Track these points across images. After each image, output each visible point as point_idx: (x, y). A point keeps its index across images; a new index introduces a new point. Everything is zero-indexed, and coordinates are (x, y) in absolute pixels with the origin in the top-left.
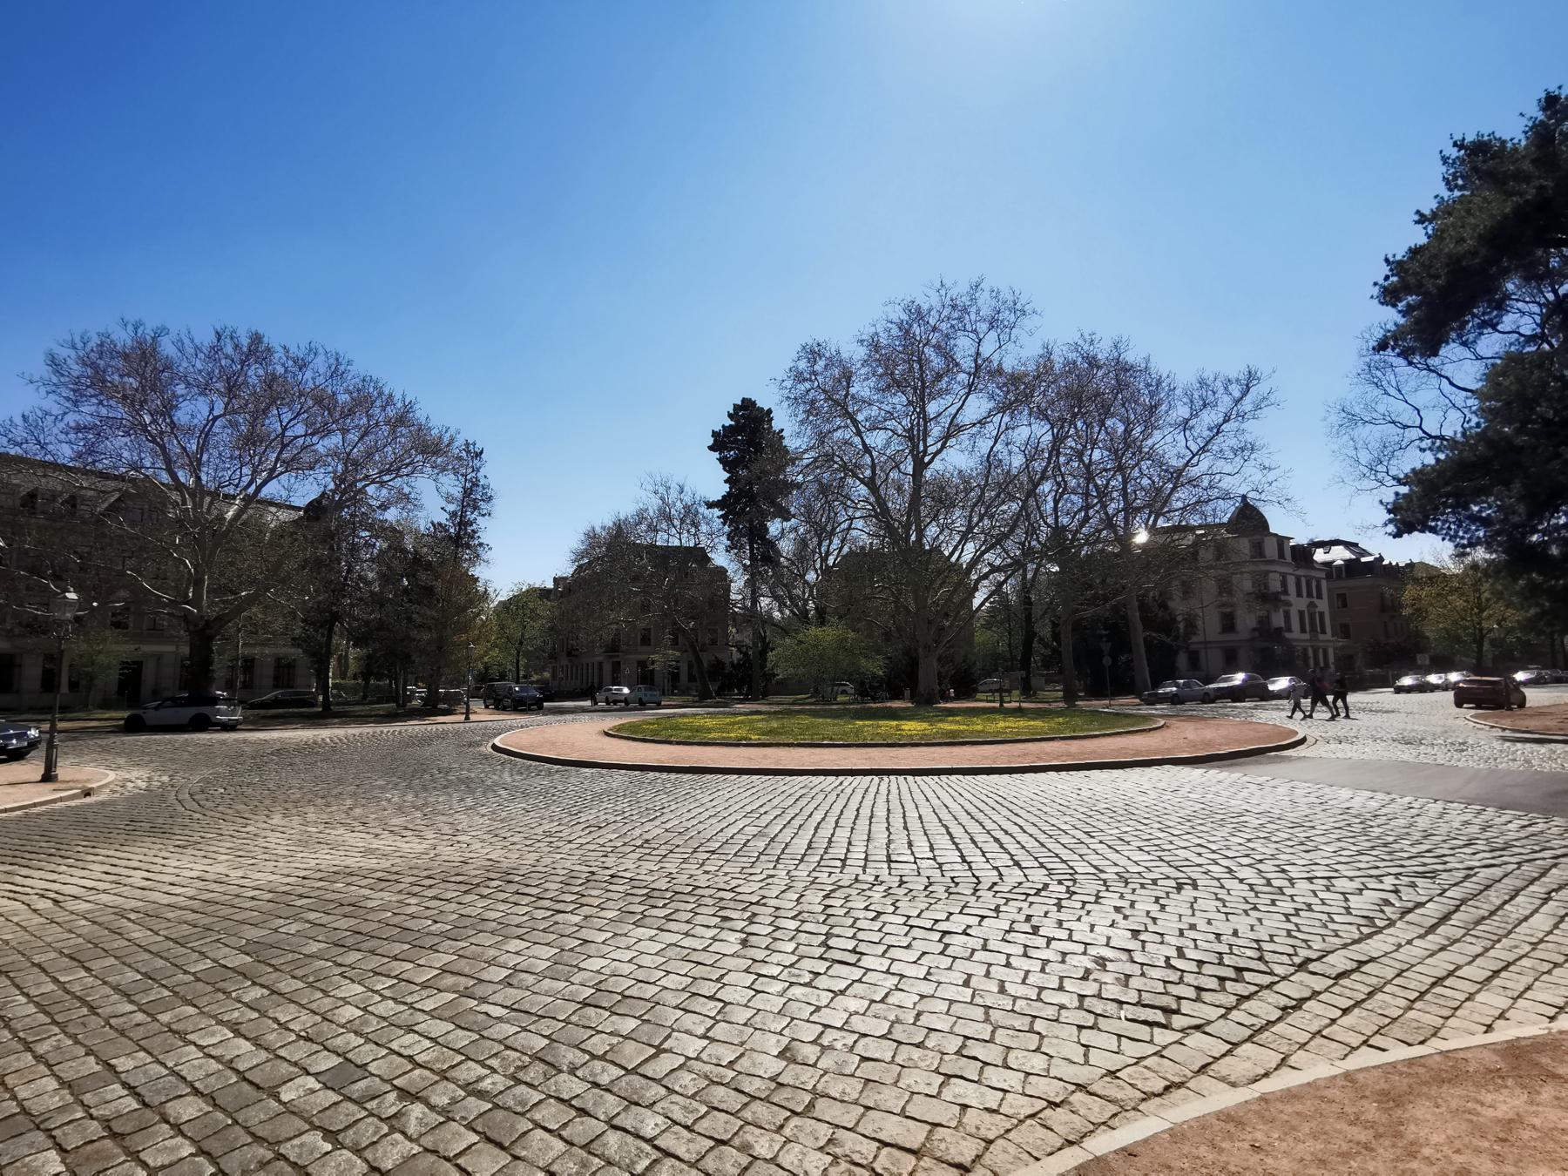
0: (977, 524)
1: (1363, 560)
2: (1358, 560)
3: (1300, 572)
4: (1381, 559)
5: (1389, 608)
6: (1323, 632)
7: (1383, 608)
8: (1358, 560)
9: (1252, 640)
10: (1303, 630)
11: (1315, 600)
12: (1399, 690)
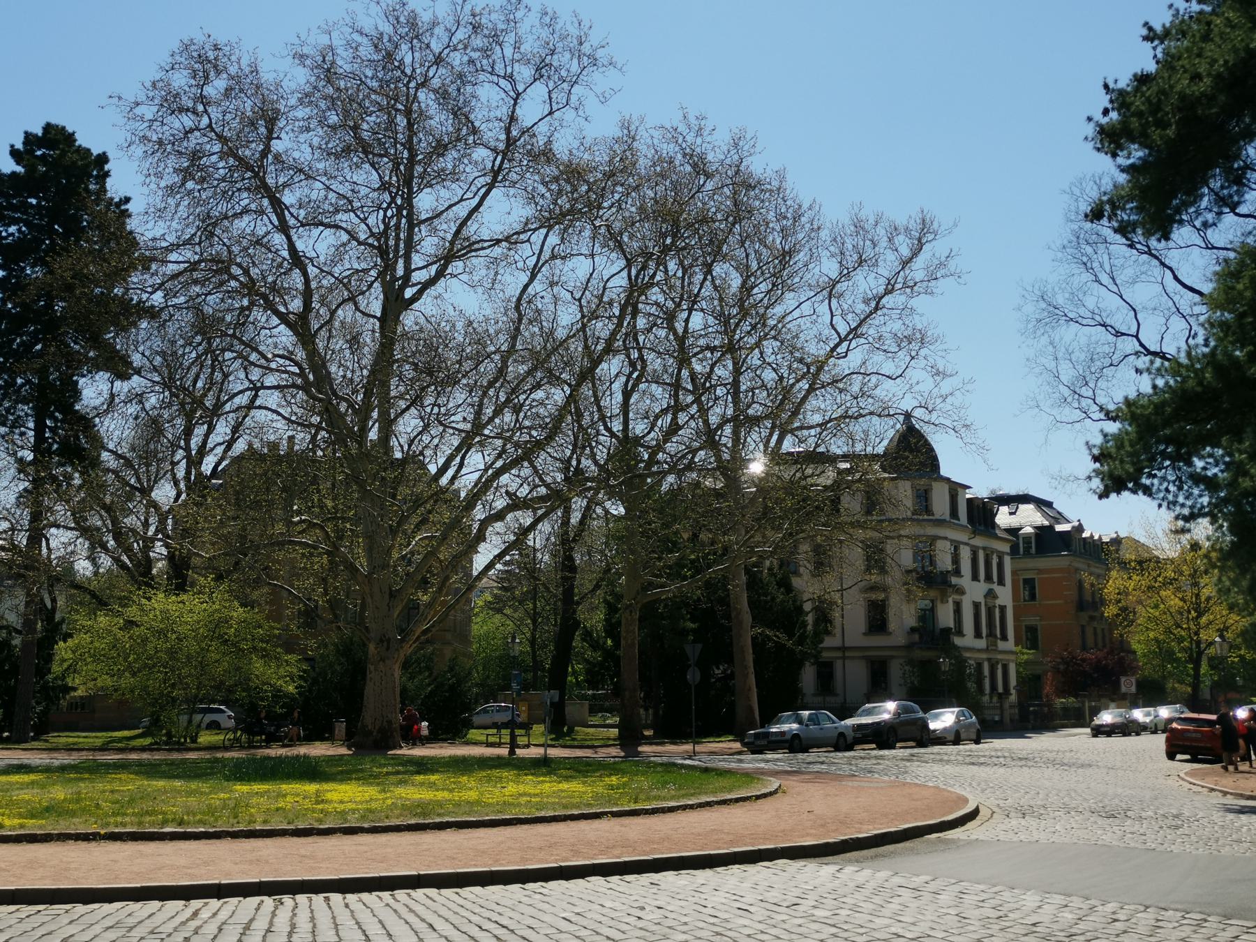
0: (491, 420)
1: (1059, 528)
2: (1051, 528)
3: (979, 541)
4: (1080, 529)
5: (1089, 603)
6: (1004, 638)
7: (1081, 605)
8: (1051, 528)
9: (909, 647)
10: (978, 635)
11: (995, 587)
12: (1099, 731)
